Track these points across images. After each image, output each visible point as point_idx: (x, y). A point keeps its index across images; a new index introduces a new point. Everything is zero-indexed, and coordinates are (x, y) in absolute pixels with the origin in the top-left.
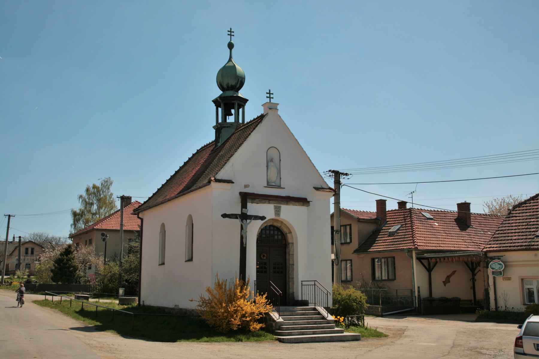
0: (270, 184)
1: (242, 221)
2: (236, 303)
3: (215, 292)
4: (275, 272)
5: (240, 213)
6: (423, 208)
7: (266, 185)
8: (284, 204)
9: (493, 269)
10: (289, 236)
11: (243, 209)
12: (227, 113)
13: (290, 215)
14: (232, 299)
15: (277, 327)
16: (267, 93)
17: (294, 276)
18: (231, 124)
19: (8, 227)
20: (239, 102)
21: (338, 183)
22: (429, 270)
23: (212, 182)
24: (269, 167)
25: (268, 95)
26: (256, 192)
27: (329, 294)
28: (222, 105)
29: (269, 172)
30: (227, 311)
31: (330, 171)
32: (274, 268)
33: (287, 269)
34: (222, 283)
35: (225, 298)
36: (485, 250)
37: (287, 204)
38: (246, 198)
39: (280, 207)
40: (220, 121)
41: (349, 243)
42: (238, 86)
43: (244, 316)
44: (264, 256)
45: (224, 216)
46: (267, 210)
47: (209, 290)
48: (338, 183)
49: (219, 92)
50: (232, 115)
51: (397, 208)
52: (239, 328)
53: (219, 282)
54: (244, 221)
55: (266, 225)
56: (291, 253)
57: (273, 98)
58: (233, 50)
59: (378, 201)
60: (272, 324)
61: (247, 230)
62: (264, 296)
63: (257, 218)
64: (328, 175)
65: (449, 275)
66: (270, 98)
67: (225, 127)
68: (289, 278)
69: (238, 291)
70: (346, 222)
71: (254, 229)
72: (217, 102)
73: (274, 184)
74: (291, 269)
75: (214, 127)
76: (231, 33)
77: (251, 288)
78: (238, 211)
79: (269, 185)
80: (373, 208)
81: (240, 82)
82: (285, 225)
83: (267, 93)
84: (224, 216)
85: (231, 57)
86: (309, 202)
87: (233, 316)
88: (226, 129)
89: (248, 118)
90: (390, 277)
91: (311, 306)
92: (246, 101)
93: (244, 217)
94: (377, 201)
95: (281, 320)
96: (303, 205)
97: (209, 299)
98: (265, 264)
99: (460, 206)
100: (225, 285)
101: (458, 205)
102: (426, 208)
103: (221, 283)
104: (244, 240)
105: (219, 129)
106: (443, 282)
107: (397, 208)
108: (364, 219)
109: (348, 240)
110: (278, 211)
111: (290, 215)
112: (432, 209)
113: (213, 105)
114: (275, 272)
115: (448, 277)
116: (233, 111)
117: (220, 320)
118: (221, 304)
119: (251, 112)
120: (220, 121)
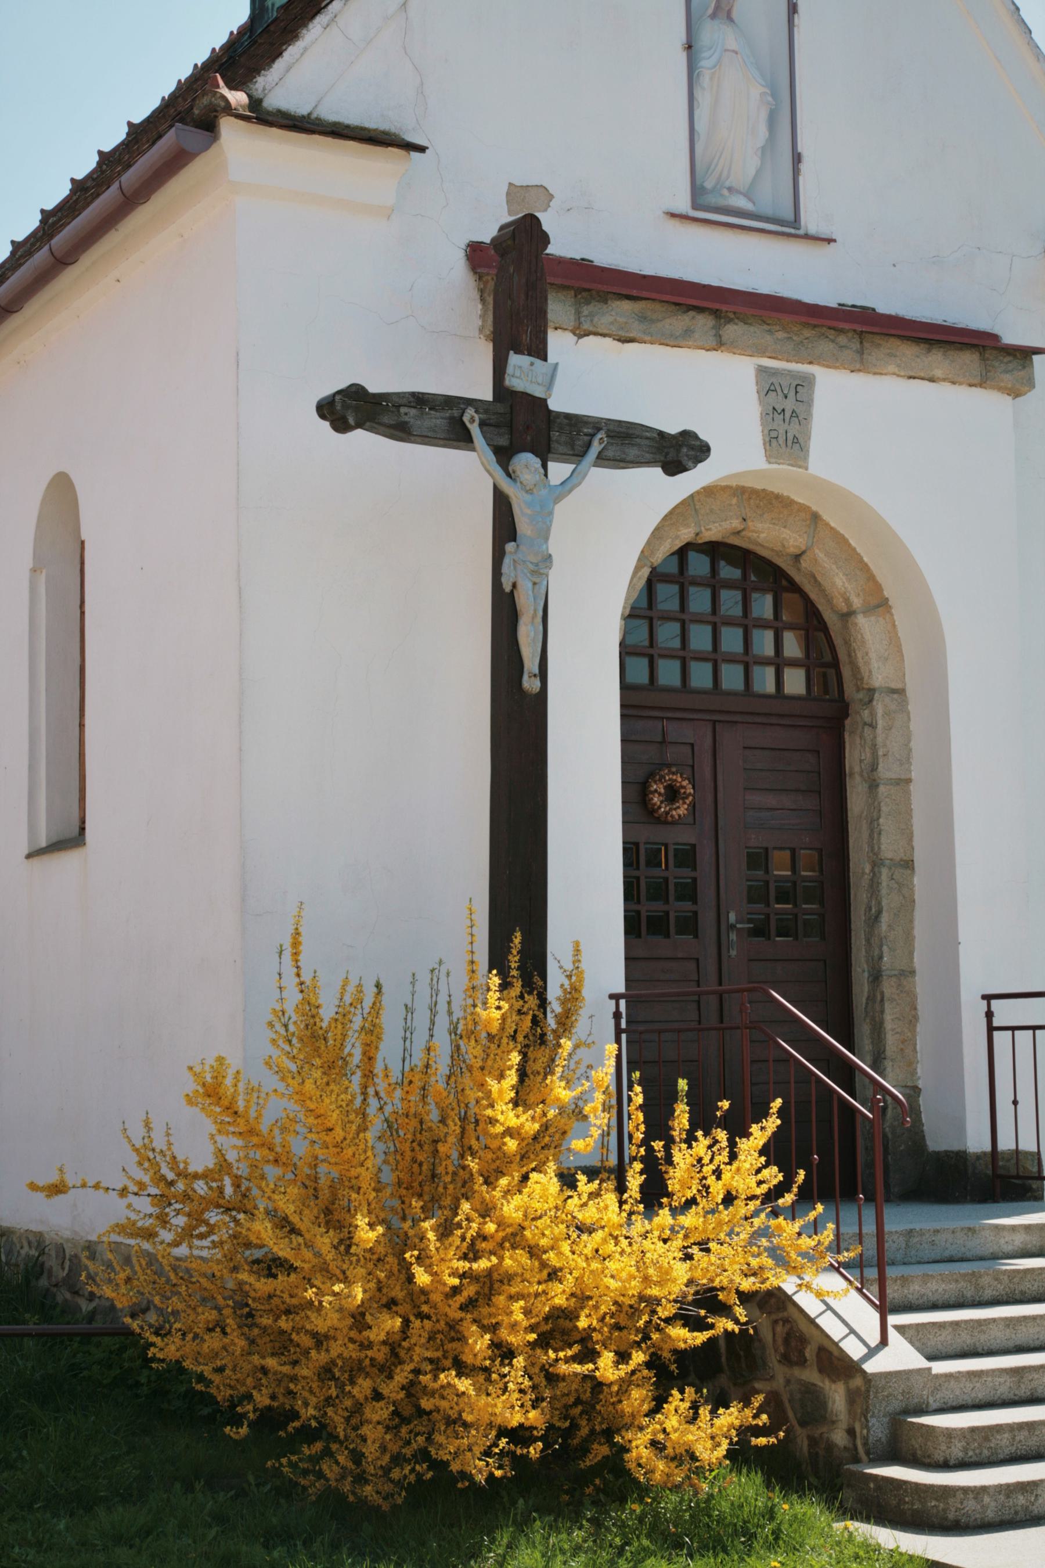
0: (712, 200)
1: (504, 455)
2: (486, 1211)
3: (276, 1108)
4: (759, 931)
5: (485, 392)
7: (683, 204)
8: (832, 363)
10: (868, 629)
11: (516, 361)
14: (437, 1166)
15: (878, 1429)
17: (919, 960)
23: (227, 126)
24: (705, 63)
26: (603, 258)
29: (704, 99)
30: (398, 1295)
32: (758, 894)
33: (859, 897)
34: (343, 1017)
35: (373, 1158)
37: (861, 365)
38: (523, 279)
39: (802, 386)
43: (556, 1329)
44: (673, 794)
45: (350, 409)
46: (704, 388)
47: (212, 1093)
52: (520, 1462)
53: (310, 1009)
54: (526, 462)
55: (686, 534)
56: (887, 770)
61: (554, 547)
62: (760, 1134)
68: (876, 977)
69: (504, 1087)
71: (603, 538)
73: (740, 202)
74: (889, 900)
77: (592, 1068)
79: (707, 206)
82: (841, 540)
84: (350, 409)
87: (454, 1333)
93: (524, 428)
95: (900, 1357)
96: (981, 383)
97: (223, 1166)
98: (687, 857)
100: (372, 1032)
103: (327, 1013)
110: (786, 420)
117: (326, 1373)
118: (335, 1218)
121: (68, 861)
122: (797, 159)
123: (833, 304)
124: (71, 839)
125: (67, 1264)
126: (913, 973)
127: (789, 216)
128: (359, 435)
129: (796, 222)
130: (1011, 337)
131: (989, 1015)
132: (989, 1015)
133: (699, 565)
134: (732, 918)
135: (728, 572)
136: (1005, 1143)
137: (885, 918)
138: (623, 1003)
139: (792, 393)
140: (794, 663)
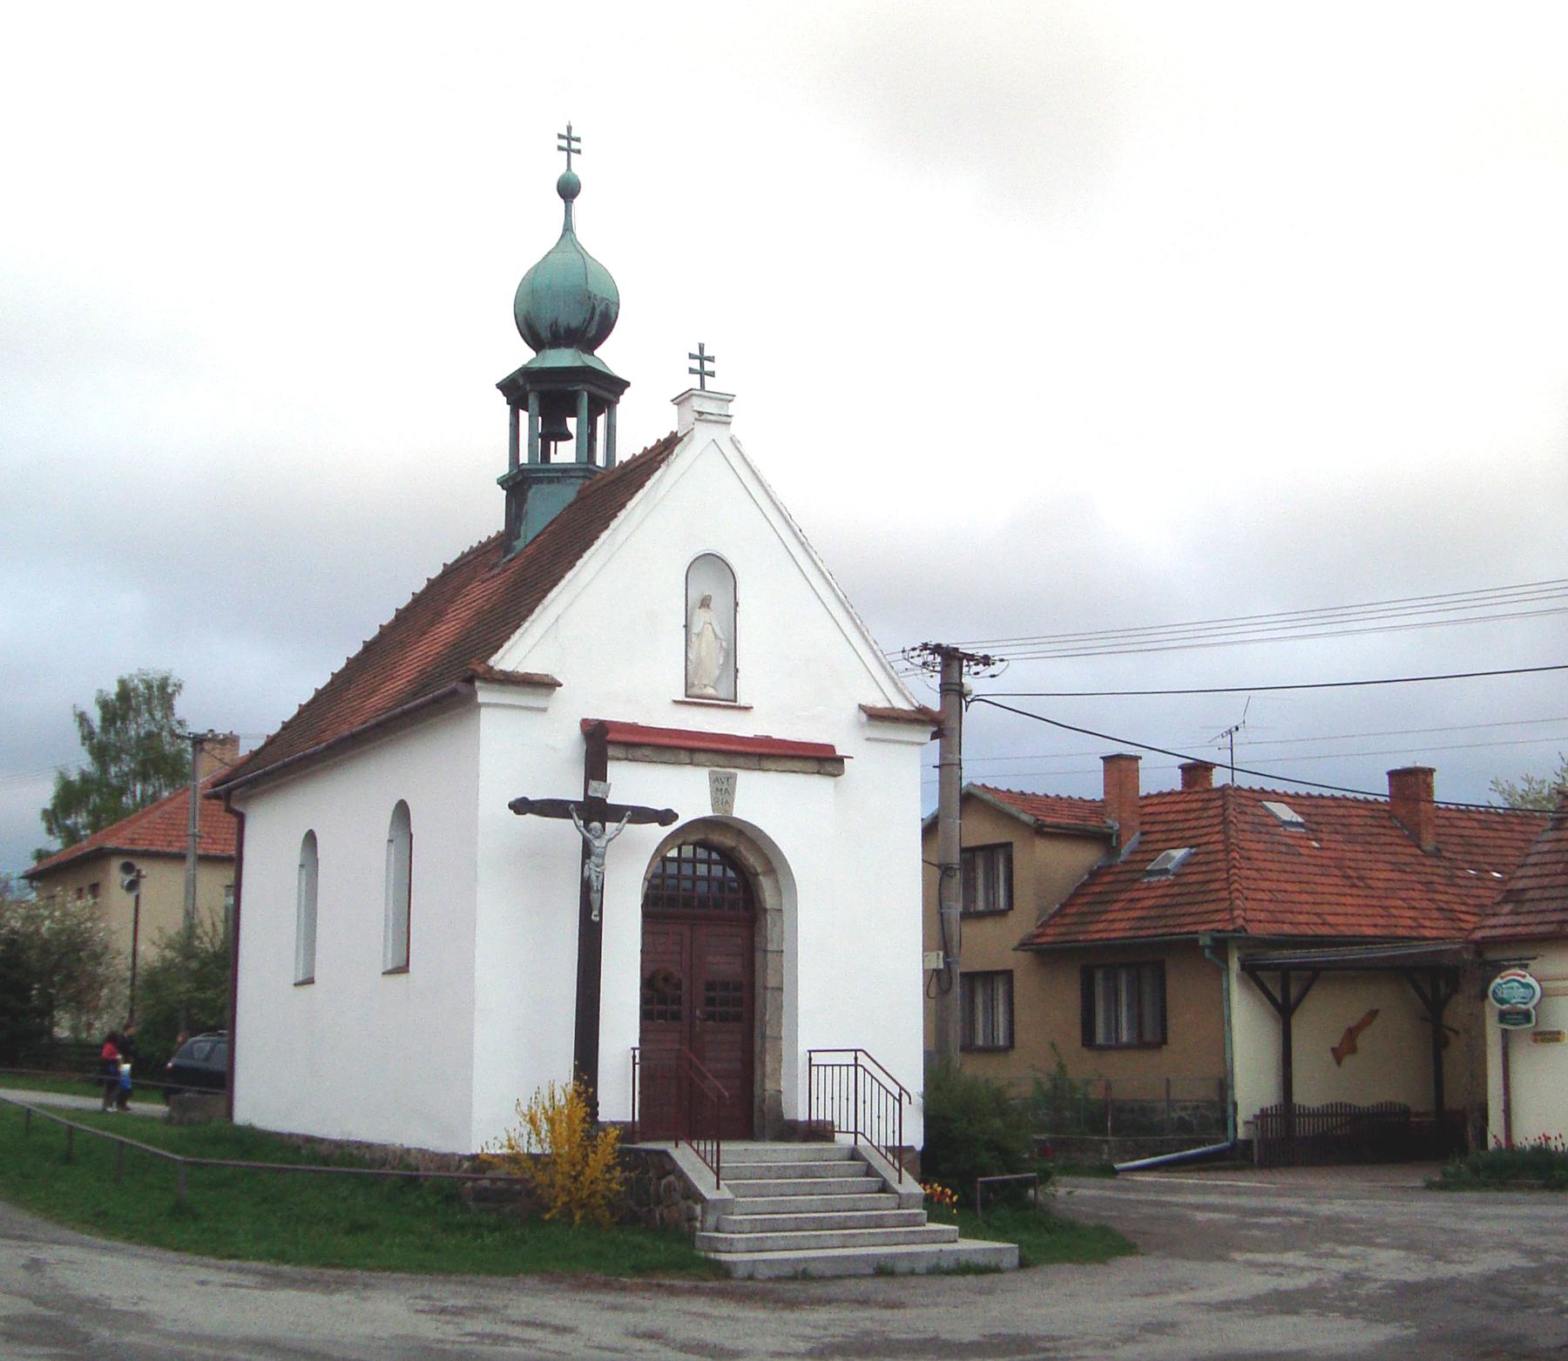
0: (696, 691)
4: (711, 1016)
5: (582, 799)
6: (1269, 785)
9: (1502, 1001)
10: (766, 883)
11: (594, 784)
12: (553, 432)
13: (762, 800)
16: (691, 356)
18: (564, 472)
19: (136, 923)
20: (594, 389)
21: (953, 691)
22: (1284, 1012)
25: (696, 364)
27: (905, 1098)
28: (533, 401)
31: (925, 647)
32: (710, 1001)
36: (1478, 935)
39: (731, 779)
40: (524, 458)
41: (1002, 913)
42: (592, 331)
45: (521, 806)
46: (686, 793)
48: (953, 691)
49: (521, 355)
50: (568, 437)
51: (1179, 788)
54: (596, 825)
57: (712, 374)
58: (577, 202)
60: (690, 1210)
63: (642, 815)
64: (919, 661)
65: (1352, 1024)
66: (702, 374)
67: (540, 481)
70: (983, 832)
72: (516, 389)
75: (503, 482)
76: (569, 143)
80: (1091, 787)
83: (691, 356)
84: (521, 806)
85: (568, 228)
86: (841, 760)
88: (545, 488)
89: (629, 446)
90: (1148, 1036)
91: (844, 1140)
92: (620, 385)
93: (595, 811)
94: (1107, 760)
99: (1399, 777)
101: (1391, 774)
102: (1280, 787)
104: (595, 896)
105: (517, 485)
106: (1333, 1050)
107: (1179, 788)
108: (1058, 826)
109: (1002, 904)
110: (723, 791)
111: (762, 800)
112: (1303, 790)
113: (501, 399)
115: (1352, 1034)
116: (572, 424)
119: (635, 427)
120: (524, 458)
121: (402, 978)
122: (737, 671)
124: (403, 969)
125: (545, 1126)
136: (814, 1118)
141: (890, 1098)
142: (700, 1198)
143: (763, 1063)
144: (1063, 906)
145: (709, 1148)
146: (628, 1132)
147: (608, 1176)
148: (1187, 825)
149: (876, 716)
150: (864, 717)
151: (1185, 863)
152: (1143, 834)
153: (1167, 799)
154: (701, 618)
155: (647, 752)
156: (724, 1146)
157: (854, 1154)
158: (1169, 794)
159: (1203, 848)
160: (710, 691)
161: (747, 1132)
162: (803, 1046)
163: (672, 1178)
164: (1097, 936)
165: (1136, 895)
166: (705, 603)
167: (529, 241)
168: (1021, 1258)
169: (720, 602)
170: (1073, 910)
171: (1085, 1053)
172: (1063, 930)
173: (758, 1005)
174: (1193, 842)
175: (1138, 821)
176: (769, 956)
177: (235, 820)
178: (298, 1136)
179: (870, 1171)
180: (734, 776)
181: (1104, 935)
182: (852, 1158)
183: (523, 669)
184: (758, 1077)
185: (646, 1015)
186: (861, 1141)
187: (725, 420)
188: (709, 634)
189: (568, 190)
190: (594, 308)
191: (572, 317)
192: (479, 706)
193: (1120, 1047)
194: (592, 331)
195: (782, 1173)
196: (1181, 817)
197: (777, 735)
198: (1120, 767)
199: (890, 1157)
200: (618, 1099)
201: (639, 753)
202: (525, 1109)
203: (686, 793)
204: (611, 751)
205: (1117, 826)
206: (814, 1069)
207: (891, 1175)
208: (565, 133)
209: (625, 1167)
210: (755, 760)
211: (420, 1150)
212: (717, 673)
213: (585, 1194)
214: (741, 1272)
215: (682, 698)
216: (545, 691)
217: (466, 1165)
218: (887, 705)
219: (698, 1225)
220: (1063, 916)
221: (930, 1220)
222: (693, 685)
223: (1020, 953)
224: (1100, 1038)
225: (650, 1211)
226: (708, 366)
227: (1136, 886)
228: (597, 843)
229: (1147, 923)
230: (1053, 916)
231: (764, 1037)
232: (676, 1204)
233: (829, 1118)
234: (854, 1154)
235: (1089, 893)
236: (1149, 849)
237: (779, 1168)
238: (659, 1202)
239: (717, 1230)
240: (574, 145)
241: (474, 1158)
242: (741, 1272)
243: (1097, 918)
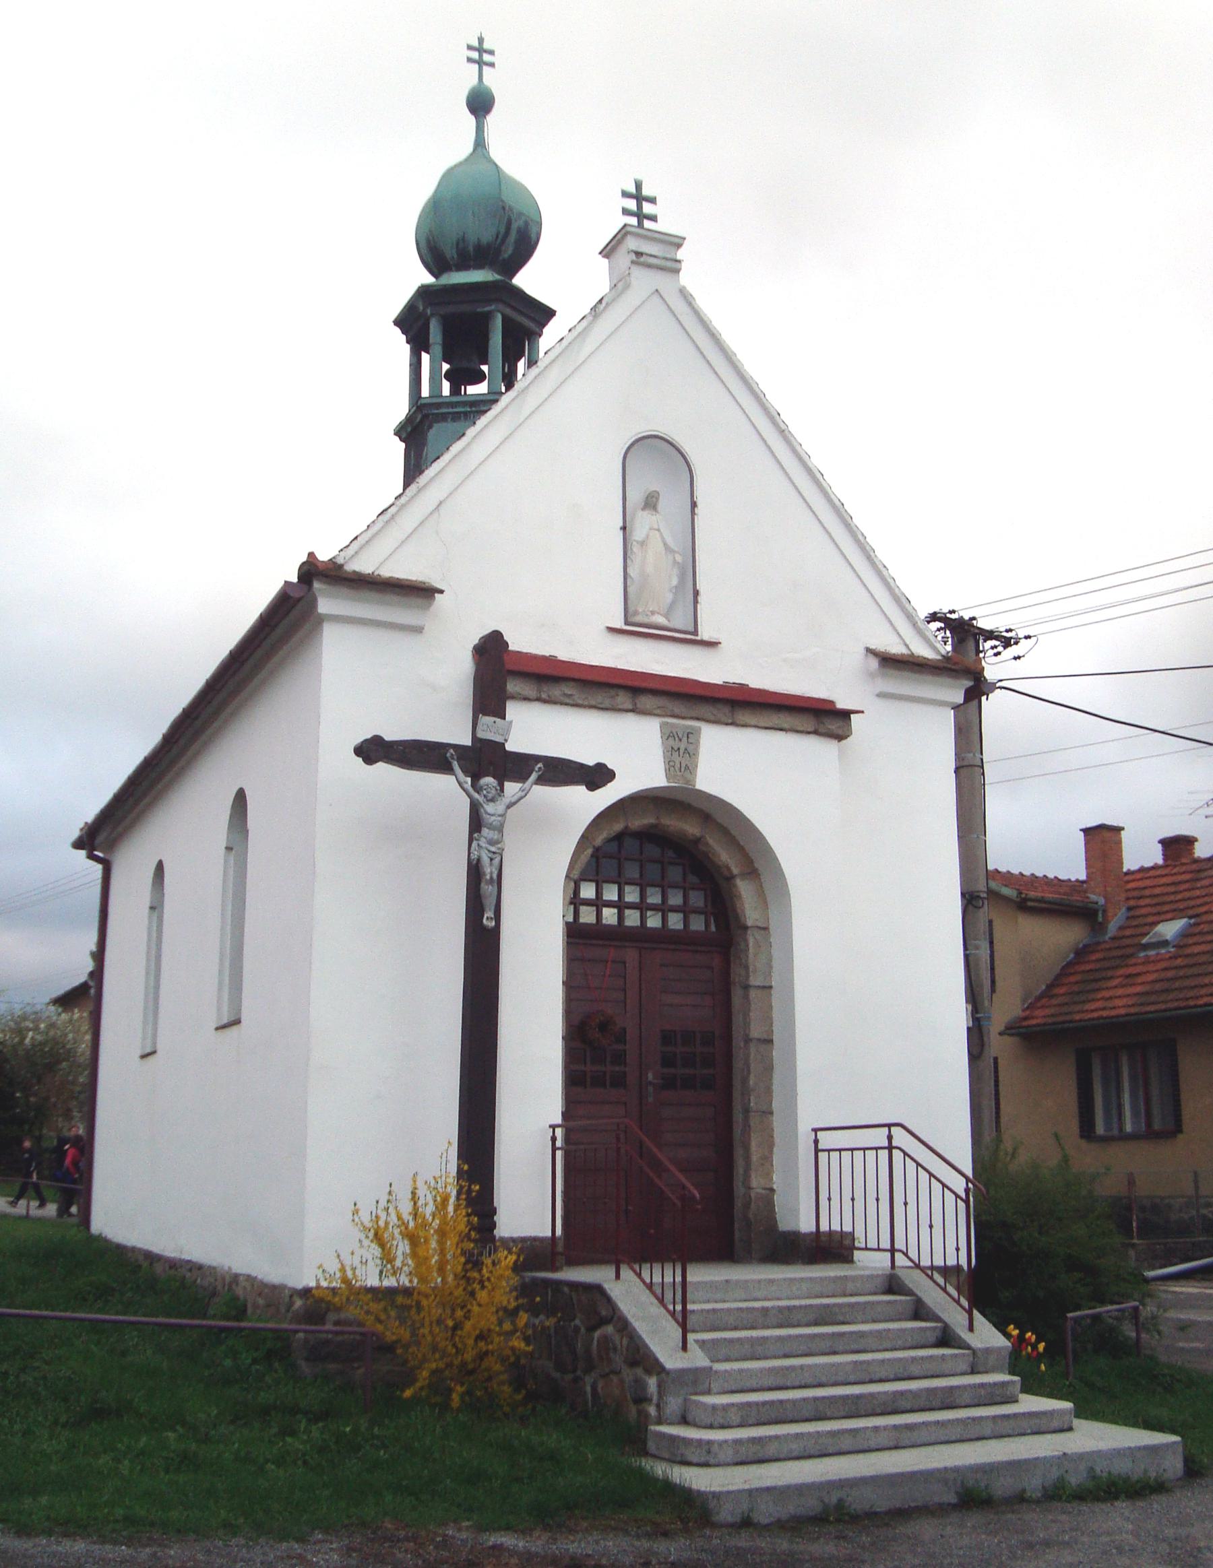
1: (476, 778)
4: (669, 1083)
10: (744, 888)
11: (485, 720)
13: (737, 768)
17: (775, 1105)
20: (508, 311)
25: (632, 204)
32: (668, 1061)
39: (692, 736)
40: (425, 392)
42: (508, 251)
45: (373, 750)
46: (634, 753)
51: (1160, 861)
54: (489, 781)
56: (755, 980)
58: (491, 119)
59: (1090, 833)
60: (640, 1385)
63: (561, 772)
67: (443, 418)
72: (412, 323)
76: (480, 55)
78: (453, 728)
79: (633, 628)
81: (515, 238)
83: (625, 194)
84: (373, 750)
85: (480, 143)
86: (846, 715)
91: (871, 1262)
93: (488, 762)
104: (488, 890)
107: (1160, 861)
110: (681, 752)
114: (669, 1083)
122: (696, 593)
123: (721, 683)
125: (402, 1248)
126: (771, 1113)
127: (691, 629)
128: (381, 766)
129: (695, 633)
130: (841, 705)
131: (816, 1142)
132: (816, 1142)
133: (631, 845)
134: (650, 1076)
135: (653, 851)
136: (824, 1227)
137: (752, 1077)
138: (559, 1132)
139: (685, 739)
140: (696, 911)
141: (950, 1197)
142: (654, 1366)
143: (747, 1148)
144: (1050, 987)
145: (668, 1279)
146: (534, 1253)
147: (507, 1326)
148: (1179, 897)
149: (890, 662)
150: (874, 663)
151: (1184, 934)
152: (1129, 909)
153: (1151, 873)
154: (643, 524)
155: (568, 689)
156: (699, 1274)
157: (893, 1285)
158: (1153, 868)
159: (1204, 918)
160: (660, 620)
161: (724, 1250)
162: (806, 1121)
163: (609, 1329)
164: (1095, 1015)
165: (1131, 970)
166: (651, 503)
167: (430, 152)
168: (1188, 1461)
169: (672, 502)
170: (1062, 990)
171: (1083, 1143)
172: (1052, 1011)
173: (738, 1064)
174: (1190, 912)
175: (1123, 896)
176: (753, 994)
177: (100, 867)
178: (140, 1250)
179: (919, 1311)
180: (699, 730)
181: (1105, 1013)
182: (890, 1290)
183: (389, 571)
184: (739, 1169)
185: (574, 1080)
186: (900, 1260)
187: (672, 268)
188: (656, 546)
189: (480, 104)
190: (509, 223)
191: (482, 232)
192: (321, 620)
193: (1124, 1137)
194: (508, 251)
195: (786, 1317)
196: (1172, 889)
197: (754, 684)
198: (1102, 840)
199: (941, 1281)
200: (528, 1203)
201: (556, 691)
202: (366, 1218)
203: (634, 753)
204: (512, 686)
205: (1102, 901)
206: (823, 1156)
207: (956, 1317)
208: (476, 44)
209: (534, 1310)
210: (727, 709)
211: (249, 1277)
212: (669, 597)
213: (468, 1357)
214: (726, 1514)
215: (619, 624)
216: (420, 601)
217: (298, 1303)
218: (904, 651)
219: (652, 1410)
220: (1052, 997)
221: (1027, 1389)
222: (636, 613)
223: (1006, 1037)
224: (1100, 1129)
225: (576, 1380)
226: (647, 208)
227: (1133, 961)
228: (490, 808)
229: (1153, 998)
230: (1039, 999)
231: (747, 1111)
232: (618, 1373)
233: (847, 1228)
234: (893, 1285)
235: (1078, 970)
236: (1140, 921)
237: (781, 1310)
238: (590, 1368)
239: (684, 1421)
240: (486, 57)
241: (306, 1292)
242: (726, 1514)
243: (1091, 996)
